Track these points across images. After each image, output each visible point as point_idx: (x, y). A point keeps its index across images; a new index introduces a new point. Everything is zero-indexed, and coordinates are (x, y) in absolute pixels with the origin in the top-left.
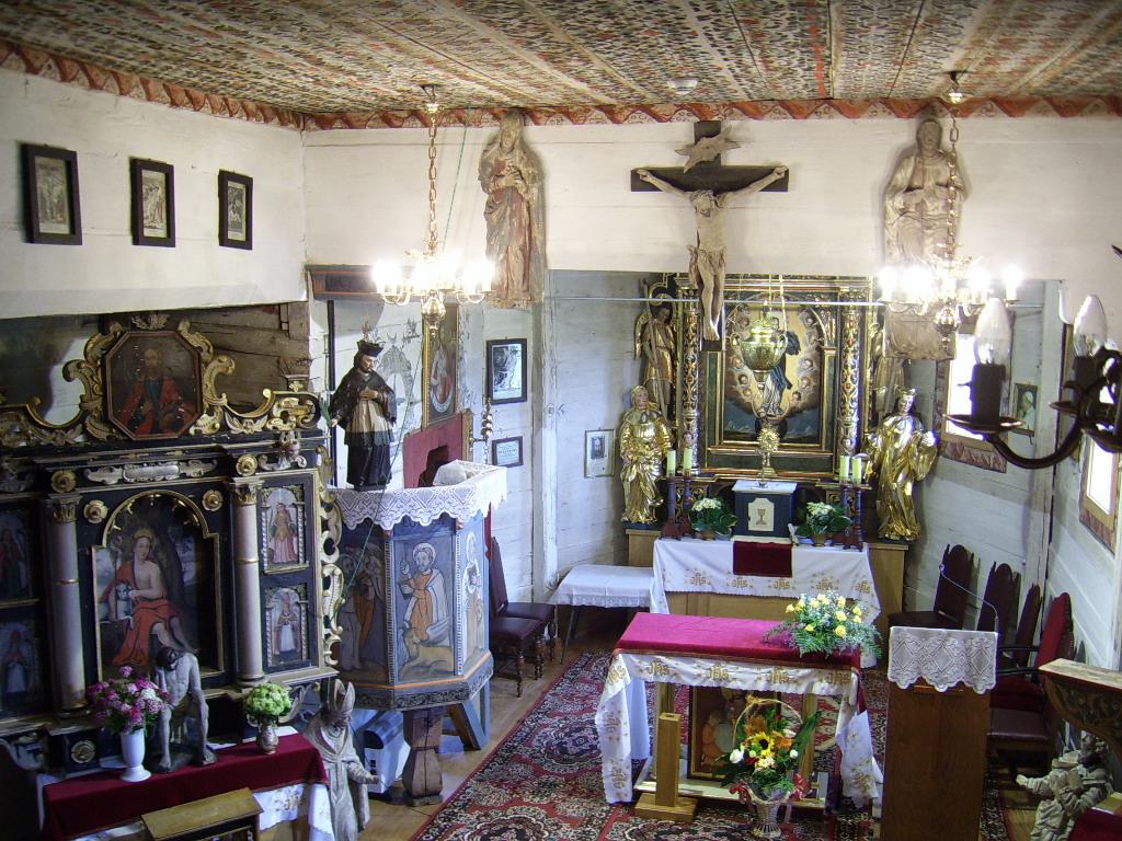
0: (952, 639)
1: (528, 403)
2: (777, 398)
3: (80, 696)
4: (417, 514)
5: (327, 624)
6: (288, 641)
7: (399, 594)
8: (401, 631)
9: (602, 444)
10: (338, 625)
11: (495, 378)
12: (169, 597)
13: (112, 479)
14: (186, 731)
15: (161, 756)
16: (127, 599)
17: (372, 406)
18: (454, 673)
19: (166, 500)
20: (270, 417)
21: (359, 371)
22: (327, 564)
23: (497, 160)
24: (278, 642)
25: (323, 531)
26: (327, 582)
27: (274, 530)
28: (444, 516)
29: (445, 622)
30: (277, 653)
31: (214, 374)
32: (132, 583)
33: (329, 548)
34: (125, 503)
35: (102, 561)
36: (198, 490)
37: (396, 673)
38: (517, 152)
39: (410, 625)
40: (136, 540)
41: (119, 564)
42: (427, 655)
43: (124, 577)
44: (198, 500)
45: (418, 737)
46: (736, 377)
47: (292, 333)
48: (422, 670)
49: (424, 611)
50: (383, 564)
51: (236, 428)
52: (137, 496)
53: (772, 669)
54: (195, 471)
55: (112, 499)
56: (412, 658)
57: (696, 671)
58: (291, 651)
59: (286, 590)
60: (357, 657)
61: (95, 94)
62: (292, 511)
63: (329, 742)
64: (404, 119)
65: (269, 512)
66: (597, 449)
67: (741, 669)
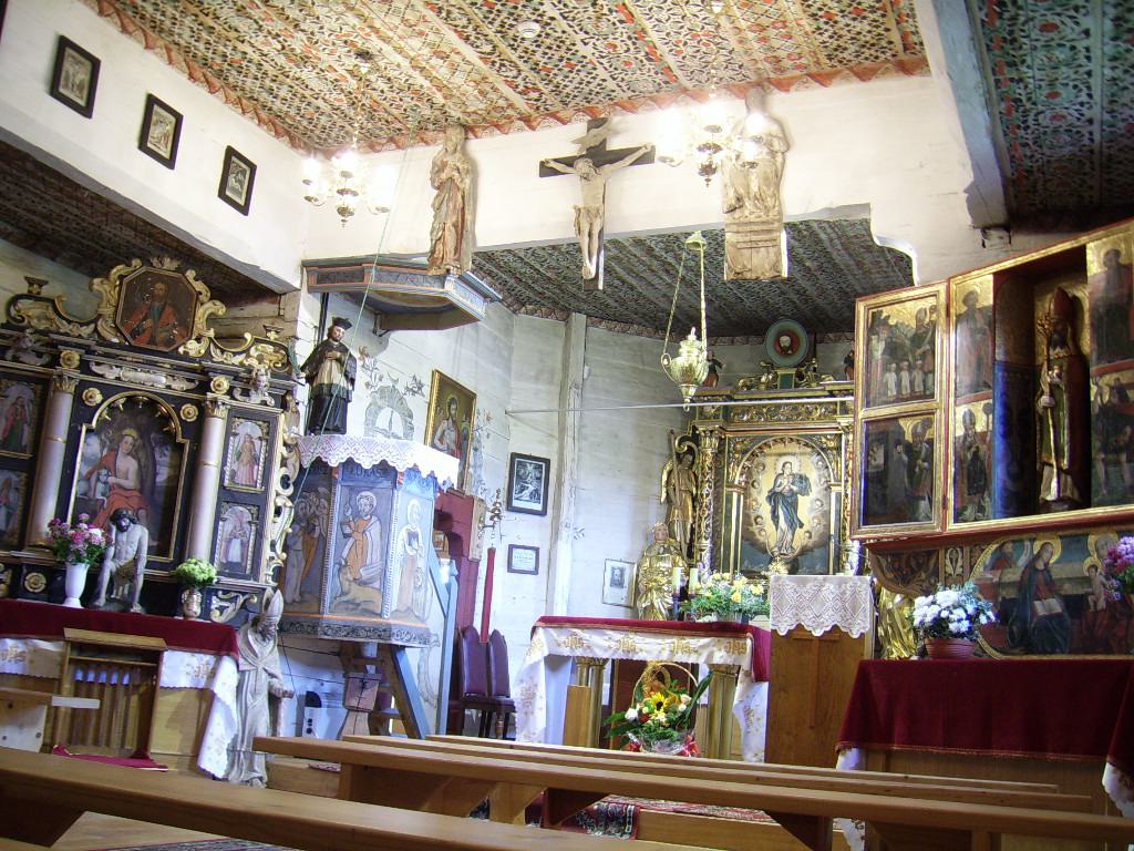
0: (827, 585)
1: (548, 519)
2: (790, 537)
3: (44, 536)
4: (361, 457)
5: (273, 545)
6: (235, 554)
7: (340, 533)
8: (337, 566)
9: (622, 575)
10: (284, 551)
11: (516, 488)
12: (141, 491)
13: (110, 374)
14: (126, 592)
15: (98, 596)
16: (105, 483)
17: (335, 365)
18: (380, 615)
19: (152, 404)
20: (248, 356)
21: (331, 340)
22: (279, 495)
23: (442, 161)
24: (227, 552)
25: (281, 466)
26: (278, 512)
27: (239, 455)
28: (384, 463)
29: (378, 565)
30: (224, 561)
31: (208, 313)
32: (113, 471)
33: (285, 481)
34: (117, 396)
35: (90, 447)
36: (179, 402)
37: (327, 604)
38: (458, 155)
39: (346, 562)
40: (123, 436)
41: (105, 453)
42: (357, 593)
43: (106, 464)
44: (178, 410)
45: (352, 696)
46: (753, 518)
47: (287, 316)
48: (351, 606)
49: (359, 552)
50: (329, 504)
51: (217, 356)
52: (127, 394)
53: (675, 640)
54: (180, 386)
55: (108, 390)
56: (343, 593)
57: (607, 644)
58: (237, 564)
59: (241, 508)
60: (298, 591)
61: (124, 37)
62: (257, 443)
63: (255, 646)
64: (383, 145)
65: (237, 439)
66: (616, 578)
67: (648, 640)
